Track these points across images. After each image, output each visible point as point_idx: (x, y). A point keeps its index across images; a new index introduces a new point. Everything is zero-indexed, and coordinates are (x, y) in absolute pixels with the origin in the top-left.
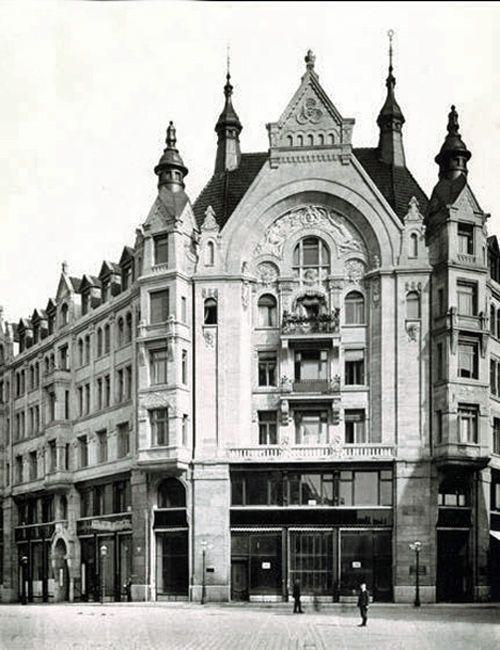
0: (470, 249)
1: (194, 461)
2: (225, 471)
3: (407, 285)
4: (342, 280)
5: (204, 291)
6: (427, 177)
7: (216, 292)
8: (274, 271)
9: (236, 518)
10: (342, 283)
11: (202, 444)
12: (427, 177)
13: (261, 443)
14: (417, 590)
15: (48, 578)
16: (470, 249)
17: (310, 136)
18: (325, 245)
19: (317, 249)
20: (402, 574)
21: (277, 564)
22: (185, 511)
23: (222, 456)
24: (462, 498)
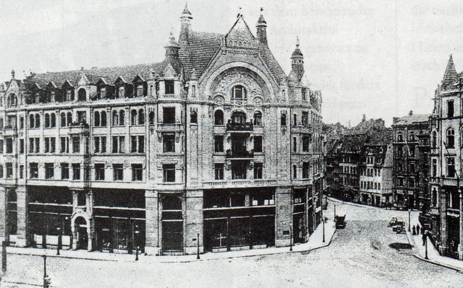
0: (304, 98)
1: (186, 189)
2: (201, 194)
3: (281, 111)
4: (252, 106)
5: (191, 108)
6: (287, 68)
7: (197, 109)
8: (222, 98)
9: (206, 214)
10: (253, 108)
11: (190, 180)
12: (287, 68)
13: (217, 178)
14: (198, 249)
15: (183, 247)
16: (304, 98)
17: (240, 42)
18: (245, 90)
19: (241, 90)
20: (320, 149)
21: (67, 216)
22: (164, 209)
23: (199, 186)
24: (300, 199)
